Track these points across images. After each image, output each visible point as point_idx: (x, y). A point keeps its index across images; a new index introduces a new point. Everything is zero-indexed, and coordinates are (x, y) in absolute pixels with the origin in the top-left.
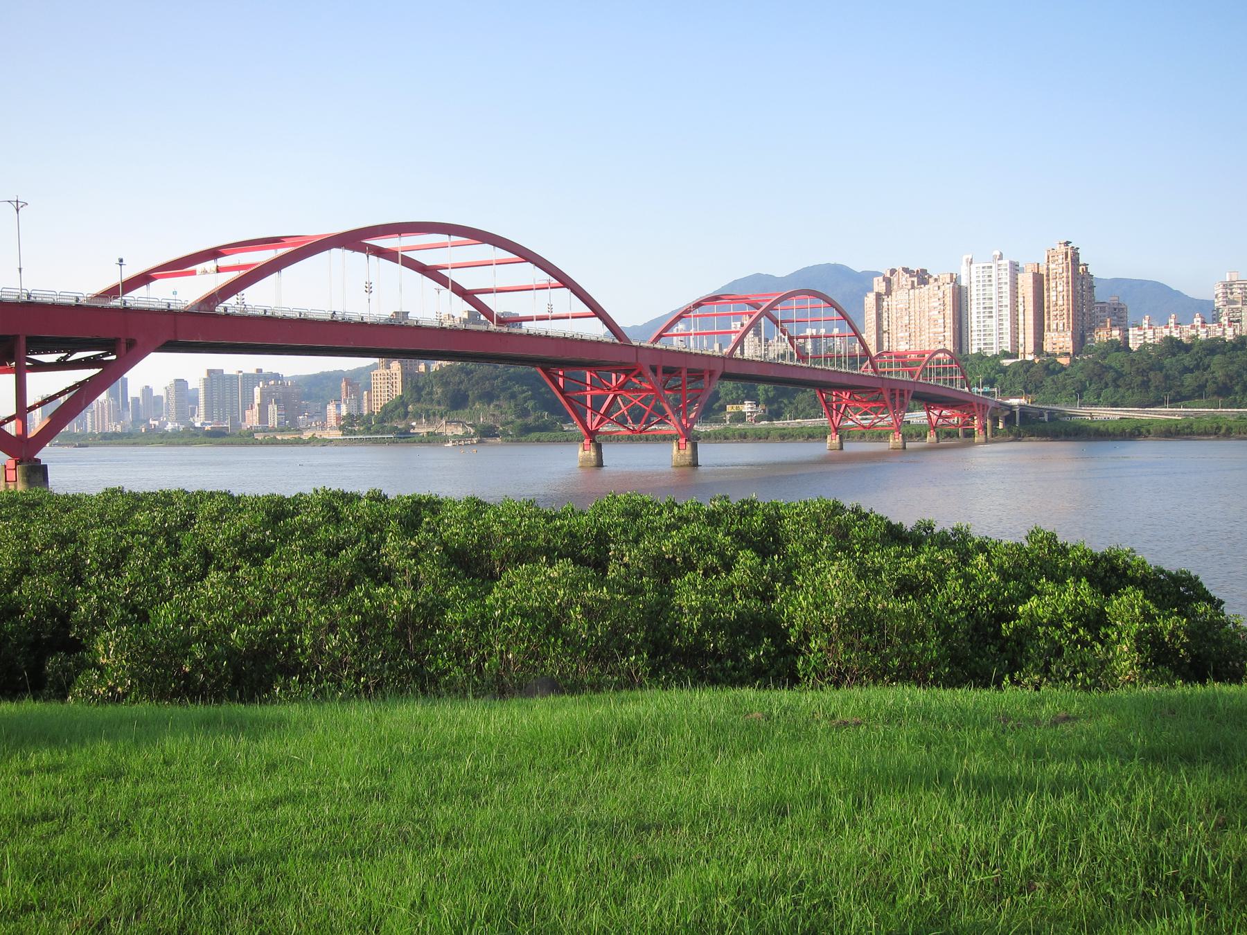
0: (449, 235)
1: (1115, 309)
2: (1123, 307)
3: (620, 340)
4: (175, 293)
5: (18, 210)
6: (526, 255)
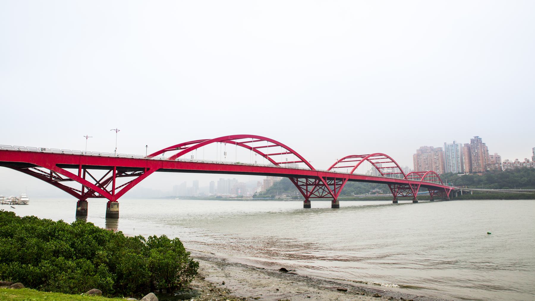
0: (253, 138)
1: (497, 157)
2: (499, 156)
3: (312, 169)
4: (227, 287)
5: (117, 132)
6: (278, 144)
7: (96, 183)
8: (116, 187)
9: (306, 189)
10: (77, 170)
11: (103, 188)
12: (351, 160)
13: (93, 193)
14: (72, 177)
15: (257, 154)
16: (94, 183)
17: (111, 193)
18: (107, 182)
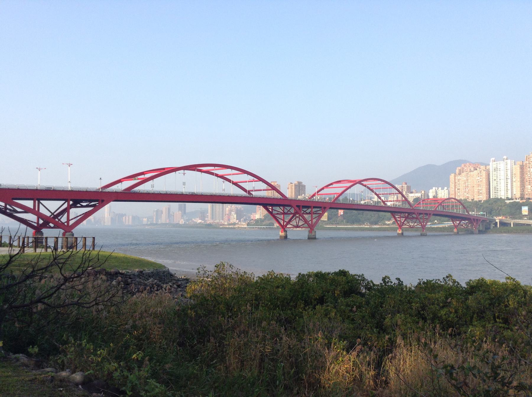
7: (51, 214)
8: (70, 218)
9: (283, 219)
10: (32, 202)
11: (58, 219)
12: (336, 186)
13: (48, 224)
14: (27, 210)
15: (225, 181)
16: (48, 214)
17: (66, 224)
18: (62, 213)
